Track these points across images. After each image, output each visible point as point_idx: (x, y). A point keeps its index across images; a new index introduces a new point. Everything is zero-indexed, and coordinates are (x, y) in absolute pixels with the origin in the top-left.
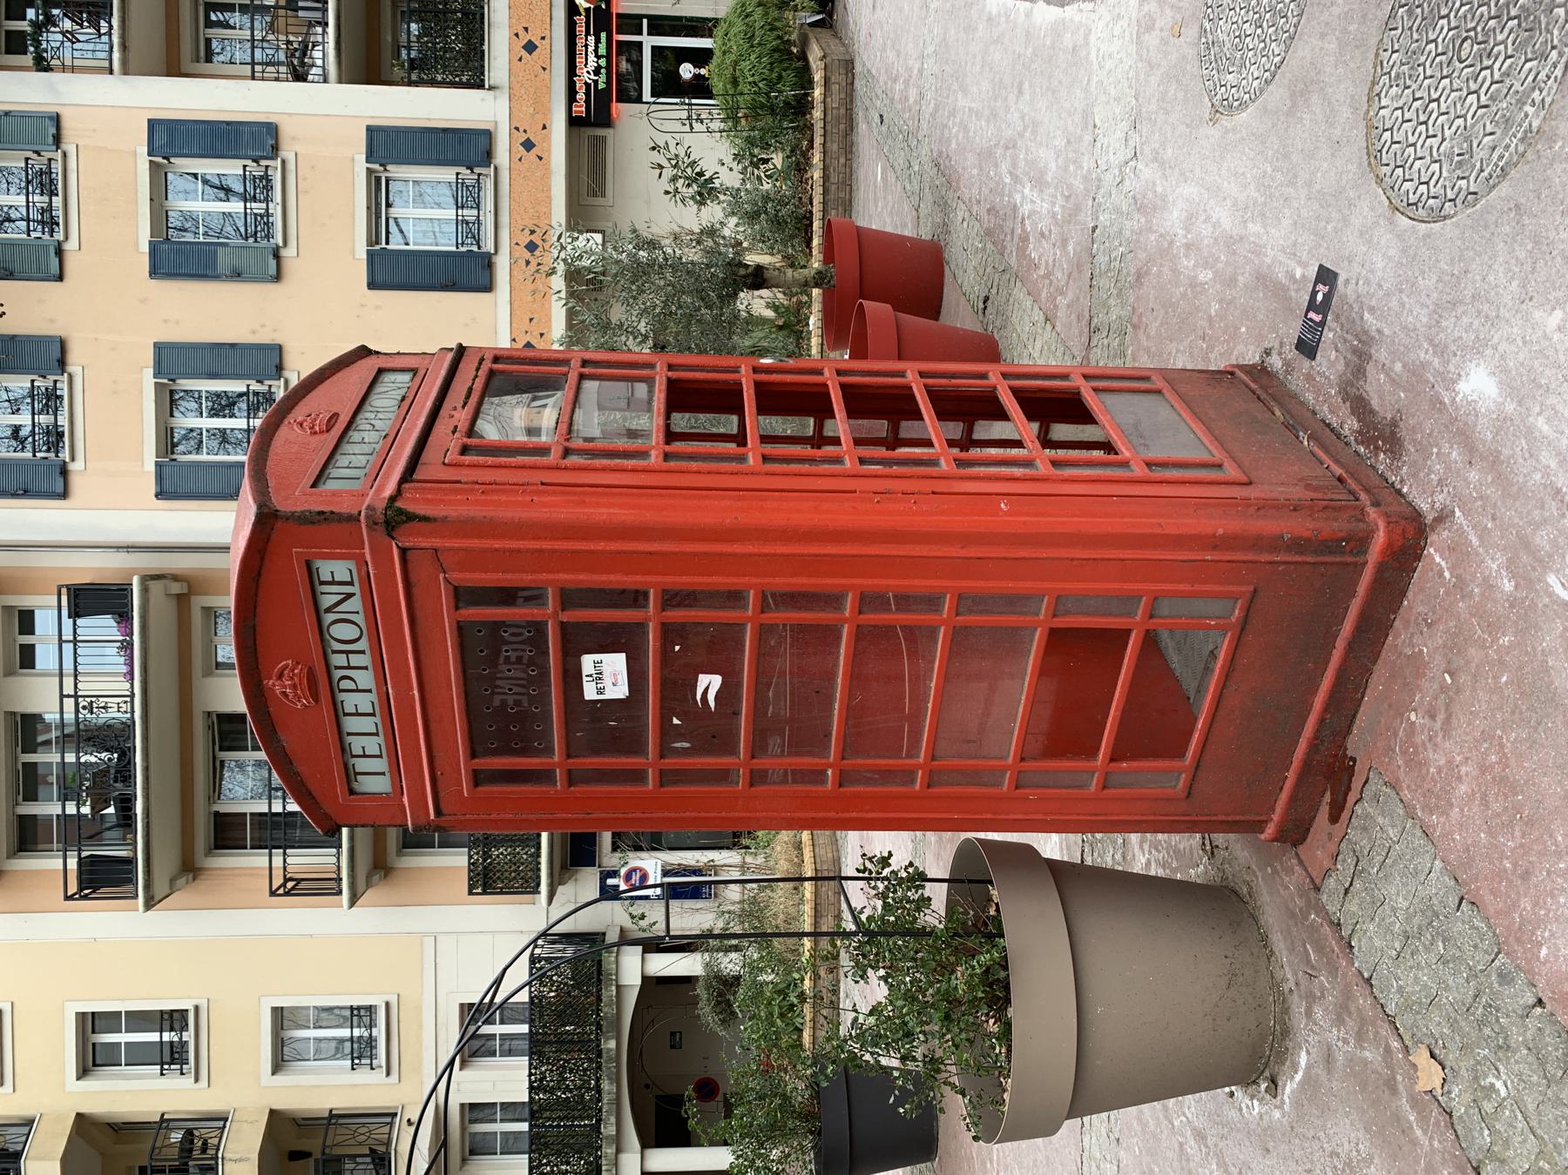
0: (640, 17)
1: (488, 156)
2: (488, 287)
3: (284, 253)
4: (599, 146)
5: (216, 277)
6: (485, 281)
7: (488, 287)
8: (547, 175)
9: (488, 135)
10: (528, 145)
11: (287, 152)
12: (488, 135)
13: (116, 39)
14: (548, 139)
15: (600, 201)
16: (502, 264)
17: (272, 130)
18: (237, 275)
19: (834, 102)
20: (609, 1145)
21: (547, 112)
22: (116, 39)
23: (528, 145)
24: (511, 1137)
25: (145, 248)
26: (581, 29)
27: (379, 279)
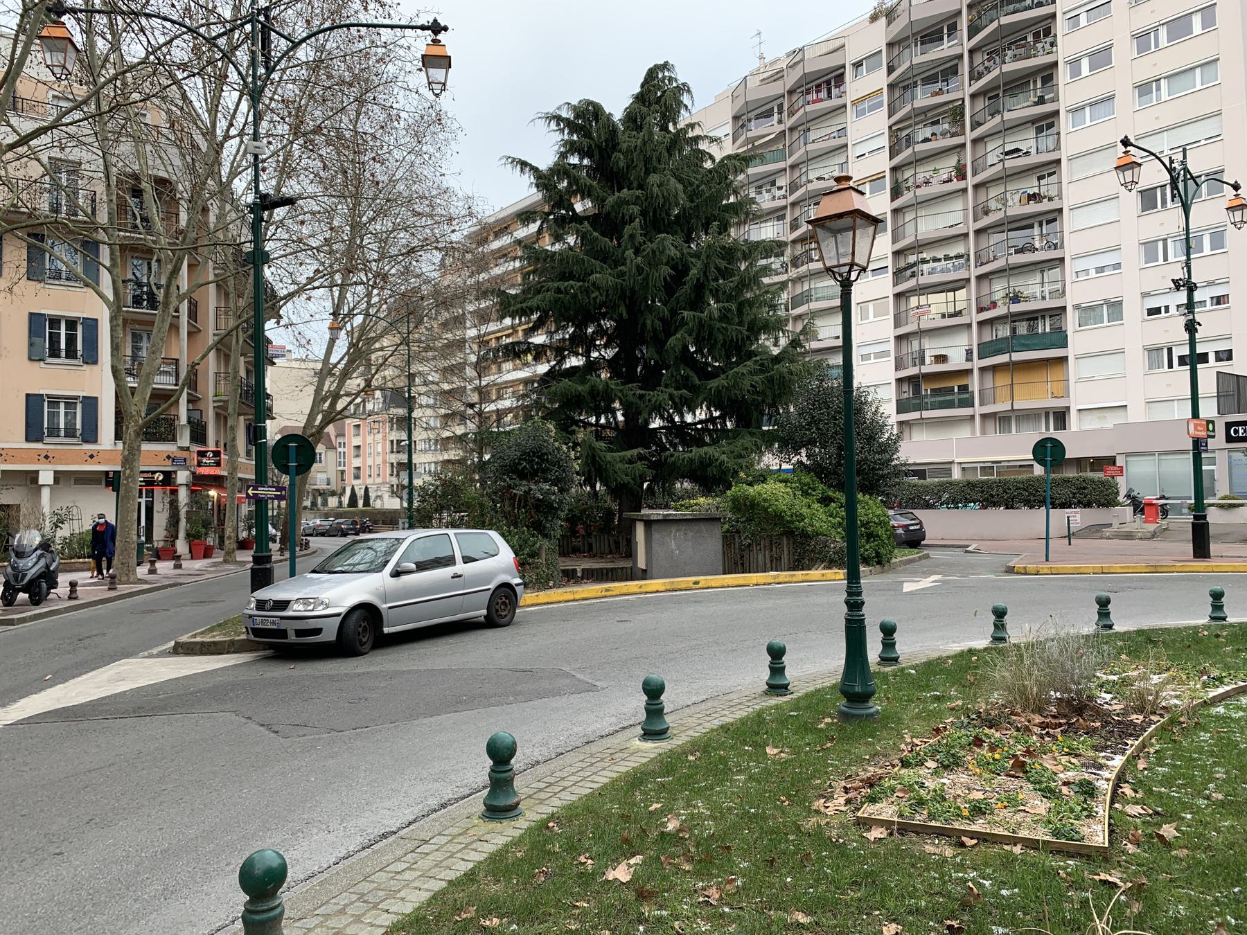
0: (153, 497)
1: (85, 441)
2: (27, 440)
3: (42, 363)
4: (98, 482)
5: (30, 337)
6: (30, 438)
7: (27, 440)
8: (78, 463)
9: (95, 441)
10: (92, 456)
11: (85, 367)
12: (95, 441)
13: (131, 309)
14: (95, 464)
15: (72, 481)
16: (39, 446)
17: (95, 362)
18: (31, 345)
19: (77, 565)
20: (1028, 330)
21: (105, 464)
22: (131, 309)
23: (92, 456)
24: (629, 578)
25: (42, 312)
26: (146, 475)
27: (30, 398)
